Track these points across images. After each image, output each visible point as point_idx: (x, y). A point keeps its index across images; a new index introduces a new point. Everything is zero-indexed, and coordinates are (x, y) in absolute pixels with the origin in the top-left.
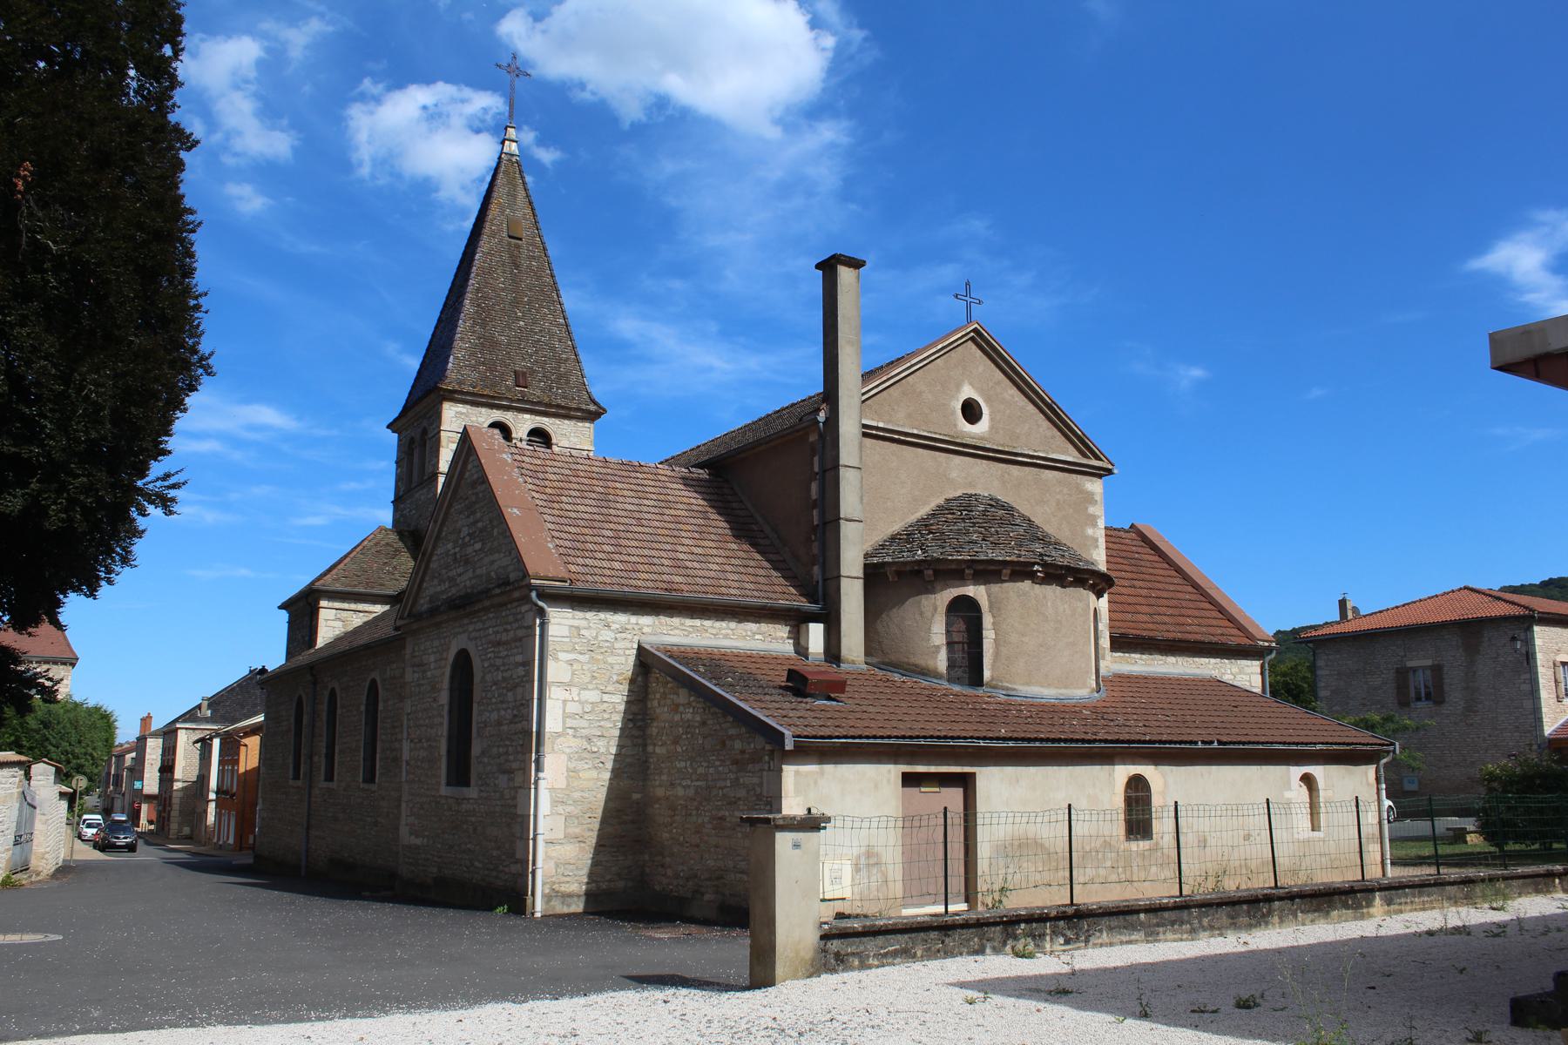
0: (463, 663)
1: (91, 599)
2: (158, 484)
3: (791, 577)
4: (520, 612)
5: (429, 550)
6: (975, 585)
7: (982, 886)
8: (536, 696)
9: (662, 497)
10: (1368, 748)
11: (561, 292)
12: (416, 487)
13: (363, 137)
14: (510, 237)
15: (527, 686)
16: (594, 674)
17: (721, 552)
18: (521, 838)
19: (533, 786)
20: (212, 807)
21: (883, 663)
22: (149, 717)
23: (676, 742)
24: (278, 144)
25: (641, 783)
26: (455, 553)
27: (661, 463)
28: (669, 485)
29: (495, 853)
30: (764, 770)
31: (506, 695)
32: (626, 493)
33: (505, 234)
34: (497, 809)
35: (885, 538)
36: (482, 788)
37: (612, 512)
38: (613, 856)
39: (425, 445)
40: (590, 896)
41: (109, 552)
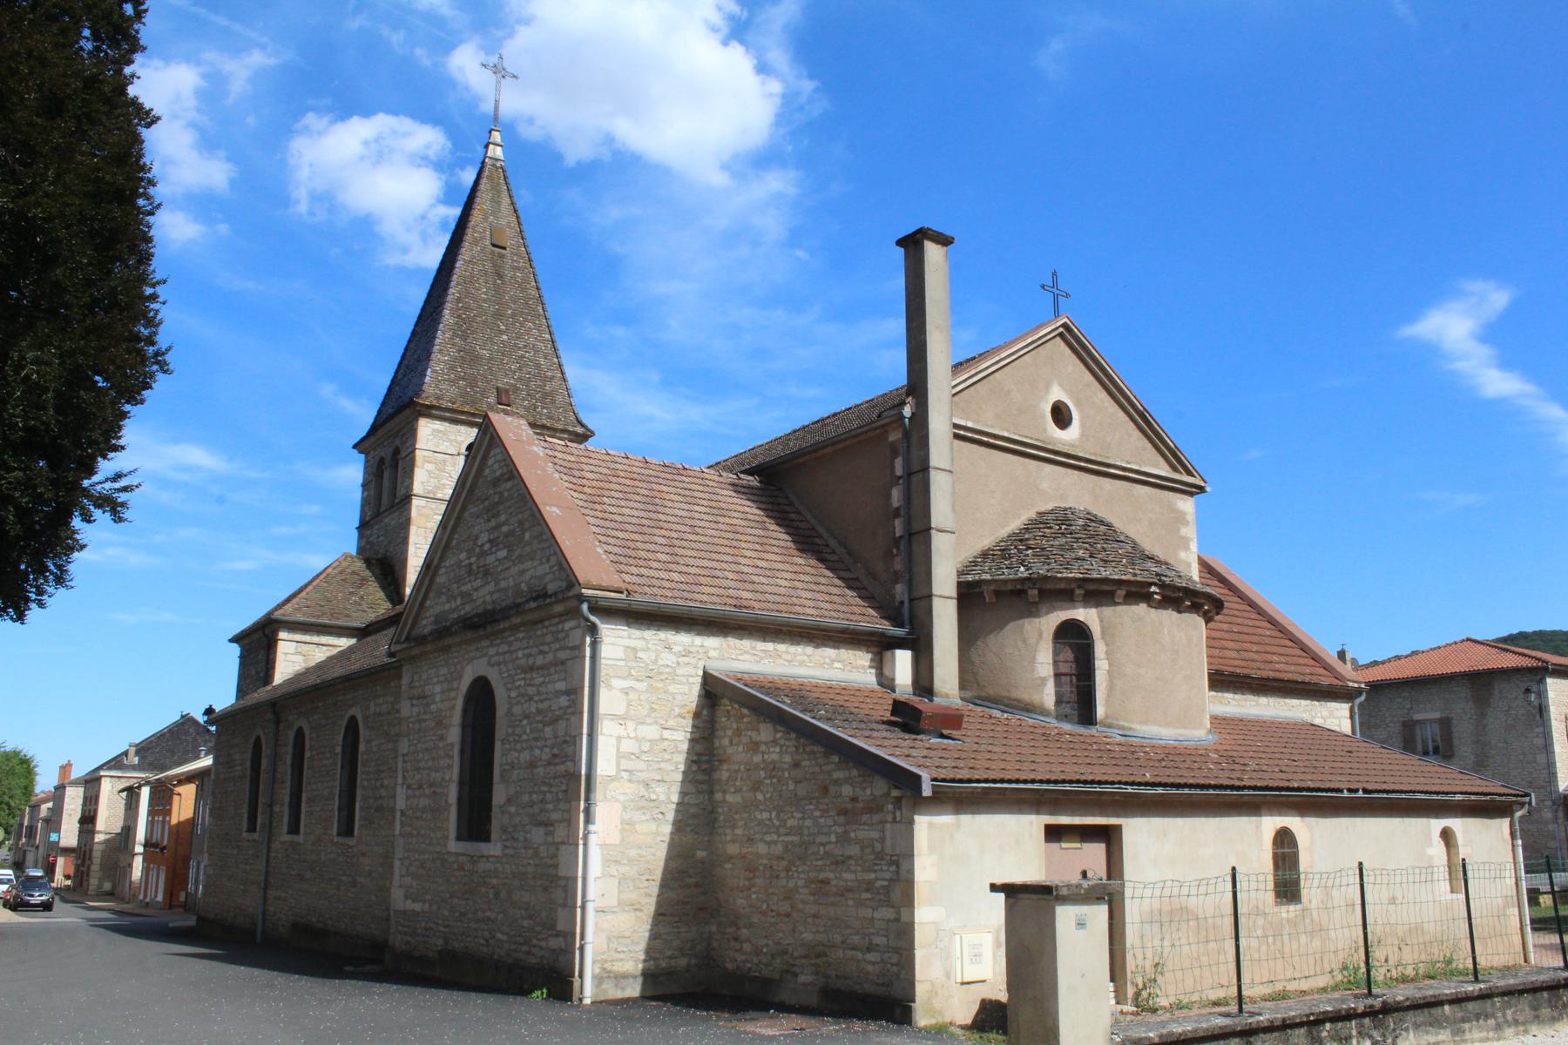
0: (481, 698)
1: (18, 624)
2: (108, 485)
3: (868, 597)
4: (563, 630)
5: (436, 562)
6: (1085, 607)
7: (1130, 964)
8: (585, 731)
9: (714, 504)
10: (1503, 798)
12: (386, 510)
13: (304, 174)
14: (494, 245)
15: (573, 719)
16: (654, 706)
17: (786, 567)
18: (564, 906)
19: (581, 842)
20: (138, 863)
21: (979, 698)
22: (69, 765)
23: (756, 787)
24: (215, 174)
25: (706, 838)
26: (471, 564)
28: (720, 491)
29: (526, 923)
30: (886, 822)
31: (543, 731)
32: (673, 497)
33: (488, 242)
34: (530, 869)
35: (975, 554)
36: (508, 844)
38: (674, 927)
39: (397, 467)
40: (649, 977)
41: (41, 570)
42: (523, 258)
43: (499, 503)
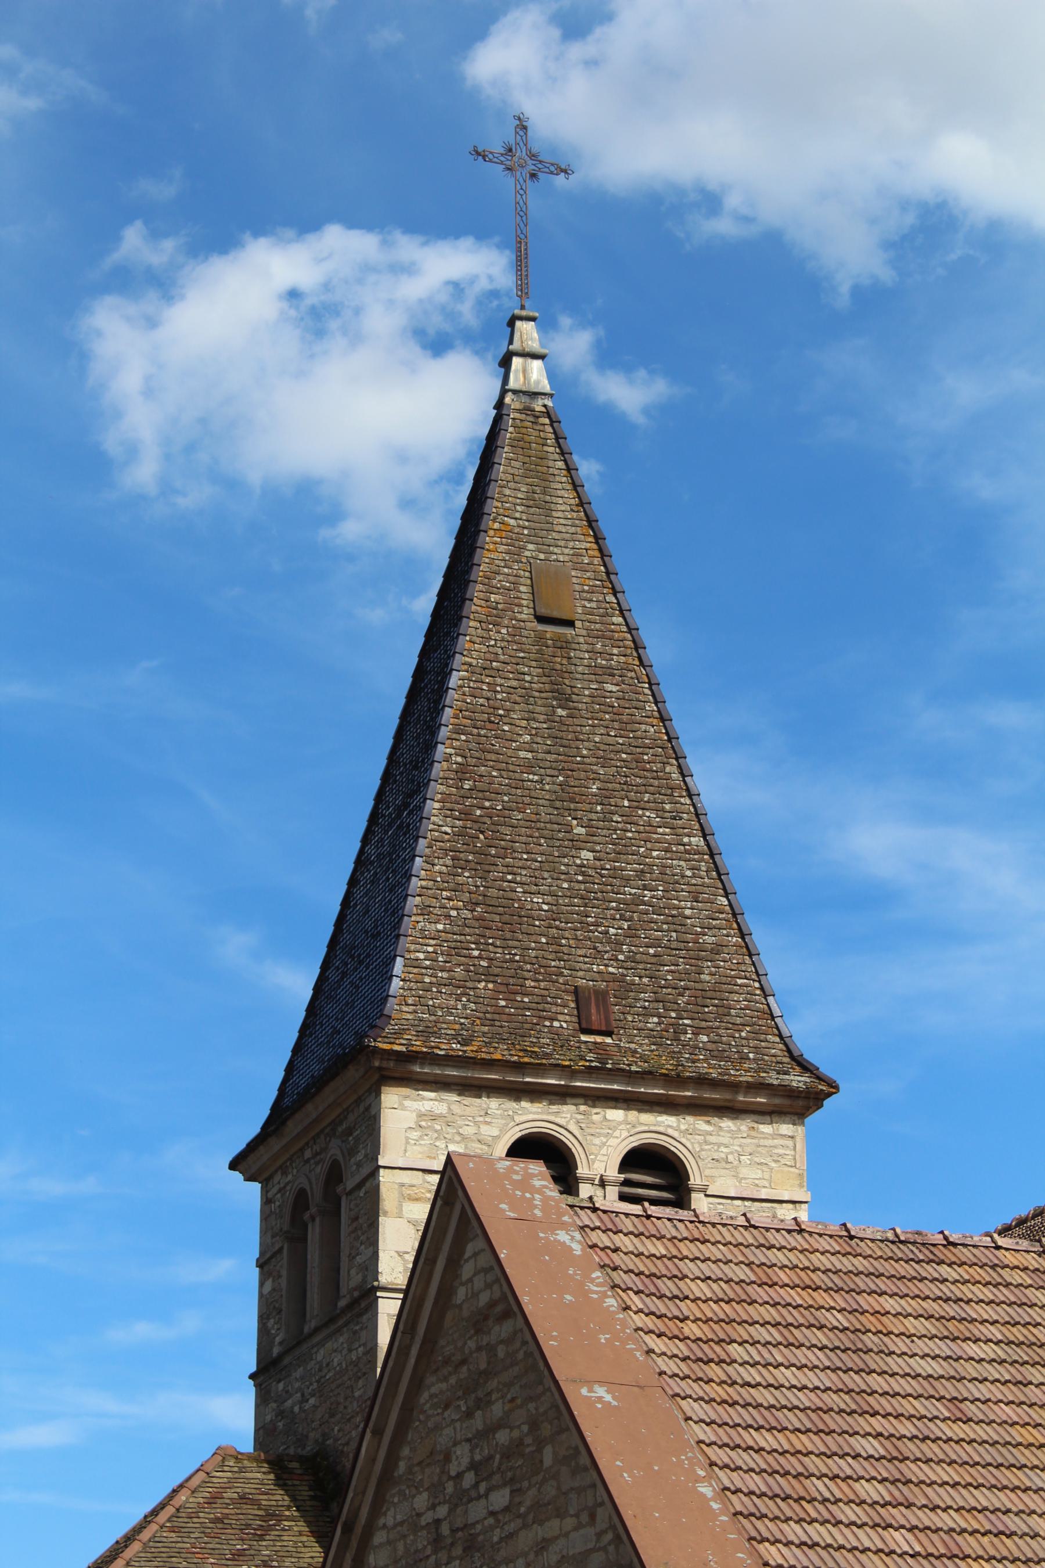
9: (1018, 1333)
11: (692, 763)
12: (317, 1330)
14: (541, 619)
26: (438, 1522)
27: (1004, 1231)
32: (911, 1325)
33: (526, 614)
37: (877, 1382)
42: (617, 643)
43: (487, 1374)
